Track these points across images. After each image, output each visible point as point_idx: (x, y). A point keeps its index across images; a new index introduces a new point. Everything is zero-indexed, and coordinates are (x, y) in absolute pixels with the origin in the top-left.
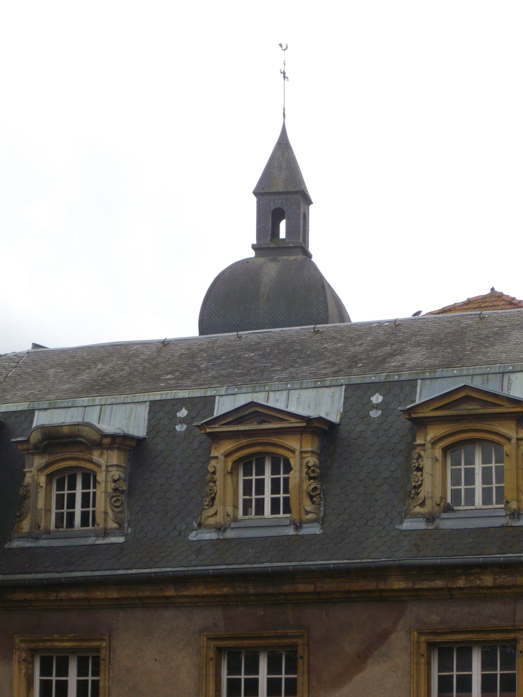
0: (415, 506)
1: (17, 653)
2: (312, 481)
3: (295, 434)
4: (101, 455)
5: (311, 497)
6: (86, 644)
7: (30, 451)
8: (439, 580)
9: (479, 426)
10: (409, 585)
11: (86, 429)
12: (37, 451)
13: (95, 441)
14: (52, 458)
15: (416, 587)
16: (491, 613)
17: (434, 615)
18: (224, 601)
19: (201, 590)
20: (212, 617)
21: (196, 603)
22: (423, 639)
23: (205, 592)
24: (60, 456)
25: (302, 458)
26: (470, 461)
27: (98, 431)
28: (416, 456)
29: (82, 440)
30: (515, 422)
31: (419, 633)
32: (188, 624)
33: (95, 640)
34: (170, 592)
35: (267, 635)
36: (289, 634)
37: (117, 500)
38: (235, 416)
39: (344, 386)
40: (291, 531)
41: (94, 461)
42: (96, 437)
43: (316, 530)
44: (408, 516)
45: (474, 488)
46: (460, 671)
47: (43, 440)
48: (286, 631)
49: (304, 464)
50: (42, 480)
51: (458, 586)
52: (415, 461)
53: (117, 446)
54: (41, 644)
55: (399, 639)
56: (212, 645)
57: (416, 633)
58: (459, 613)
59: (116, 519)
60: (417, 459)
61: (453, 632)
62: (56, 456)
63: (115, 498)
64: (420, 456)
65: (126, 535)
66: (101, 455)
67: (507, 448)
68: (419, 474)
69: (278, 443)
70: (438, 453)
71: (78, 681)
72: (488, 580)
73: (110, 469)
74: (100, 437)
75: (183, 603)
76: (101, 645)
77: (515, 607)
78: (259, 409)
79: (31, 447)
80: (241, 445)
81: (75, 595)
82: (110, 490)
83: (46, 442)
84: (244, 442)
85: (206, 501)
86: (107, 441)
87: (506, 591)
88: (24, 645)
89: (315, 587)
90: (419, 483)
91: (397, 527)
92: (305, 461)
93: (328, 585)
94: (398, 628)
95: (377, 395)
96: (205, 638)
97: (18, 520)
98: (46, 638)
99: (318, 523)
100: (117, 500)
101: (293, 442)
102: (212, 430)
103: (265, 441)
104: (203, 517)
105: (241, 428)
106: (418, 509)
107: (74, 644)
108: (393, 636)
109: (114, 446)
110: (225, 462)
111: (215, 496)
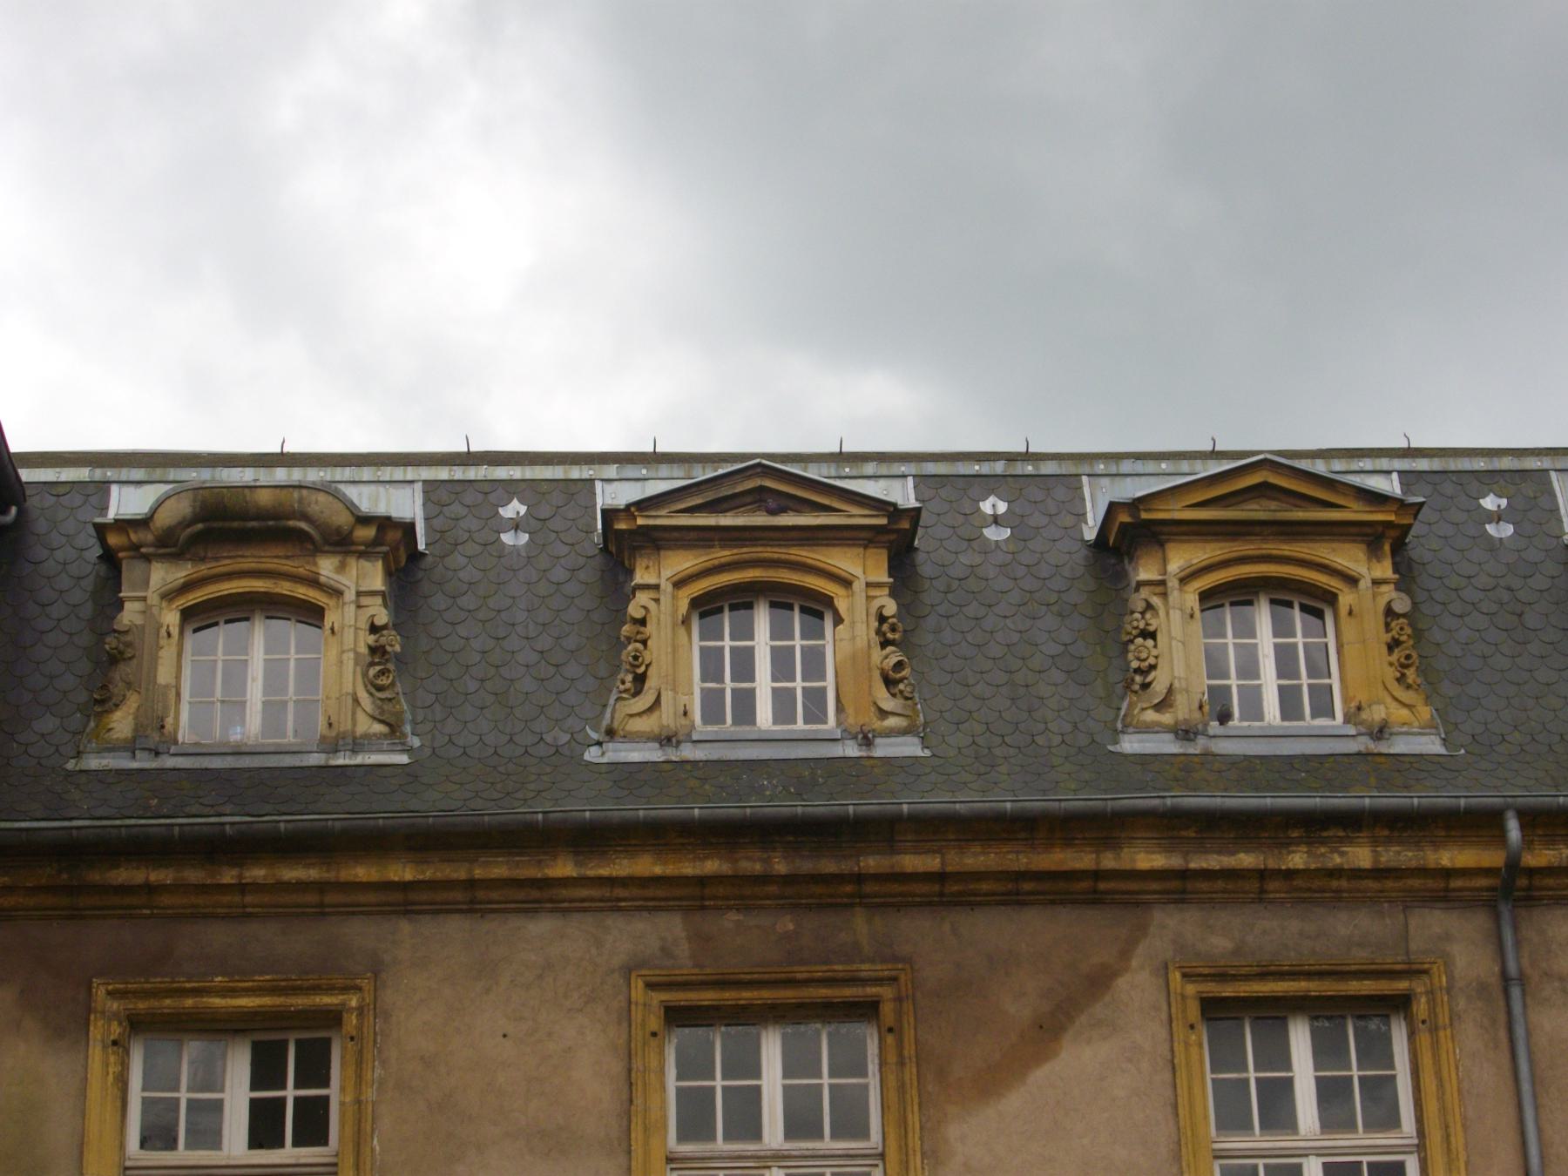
0: (1143, 709)
1: (100, 1023)
2: (890, 649)
3: (849, 545)
4: (342, 568)
5: (889, 682)
6: (299, 1002)
7: (143, 550)
8: (1247, 852)
9: (1287, 549)
10: (1174, 861)
11: (322, 497)
12: (162, 551)
13: (338, 530)
14: (204, 569)
15: (1193, 865)
16: (1350, 932)
17: (1219, 934)
18: (695, 896)
19: (645, 865)
20: (661, 934)
21: (619, 900)
22: (1191, 989)
23: (658, 870)
24: (226, 565)
25: (869, 598)
26: (210, 1079)
27: (350, 507)
28: (1141, 606)
29: (303, 525)
30: (1363, 546)
31: (1184, 975)
32: (594, 951)
33: (330, 989)
34: (563, 868)
35: (805, 975)
36: (863, 974)
37: (382, 673)
38: (710, 496)
39: (910, 479)
40: (851, 750)
41: (322, 579)
42: (343, 519)
43: (910, 748)
44: (1131, 730)
45: (1260, 686)
46: (1265, 1070)
47: (195, 519)
48: (854, 967)
49: (873, 610)
50: (171, 618)
51: (1291, 866)
52: (1137, 616)
53: (384, 549)
54: (168, 1002)
55: (1137, 988)
56: (655, 1002)
57: (1178, 975)
58: (1276, 932)
59: (382, 712)
60: (1143, 613)
61: (1263, 975)
62: (214, 564)
63: (378, 668)
64: (1149, 606)
65: (410, 751)
66: (342, 568)
67: (1346, 599)
68: (1150, 643)
69: (809, 561)
70: (1192, 600)
71: (253, 1102)
72: (1361, 855)
73: (365, 601)
74: (351, 519)
75: (583, 900)
76: (343, 1004)
77: (1406, 925)
78: (769, 483)
79: (150, 538)
80: (716, 562)
81: (293, 873)
82: (363, 650)
83: (200, 526)
84: (724, 555)
85: (623, 682)
86: (369, 533)
87: (1389, 884)
88: (115, 1005)
89: (943, 863)
90: (1152, 661)
91: (1111, 748)
92: (876, 604)
93: (976, 859)
94: (1134, 963)
95: (992, 499)
96: (640, 984)
97: (98, 709)
98: (188, 985)
99: (917, 735)
100: (382, 673)
101: (844, 560)
102: (651, 522)
103: (776, 556)
104: (619, 716)
105: (726, 520)
106: (1150, 716)
107: (267, 1001)
108: (1122, 983)
109: (379, 549)
110: (674, 597)
111: (645, 673)
